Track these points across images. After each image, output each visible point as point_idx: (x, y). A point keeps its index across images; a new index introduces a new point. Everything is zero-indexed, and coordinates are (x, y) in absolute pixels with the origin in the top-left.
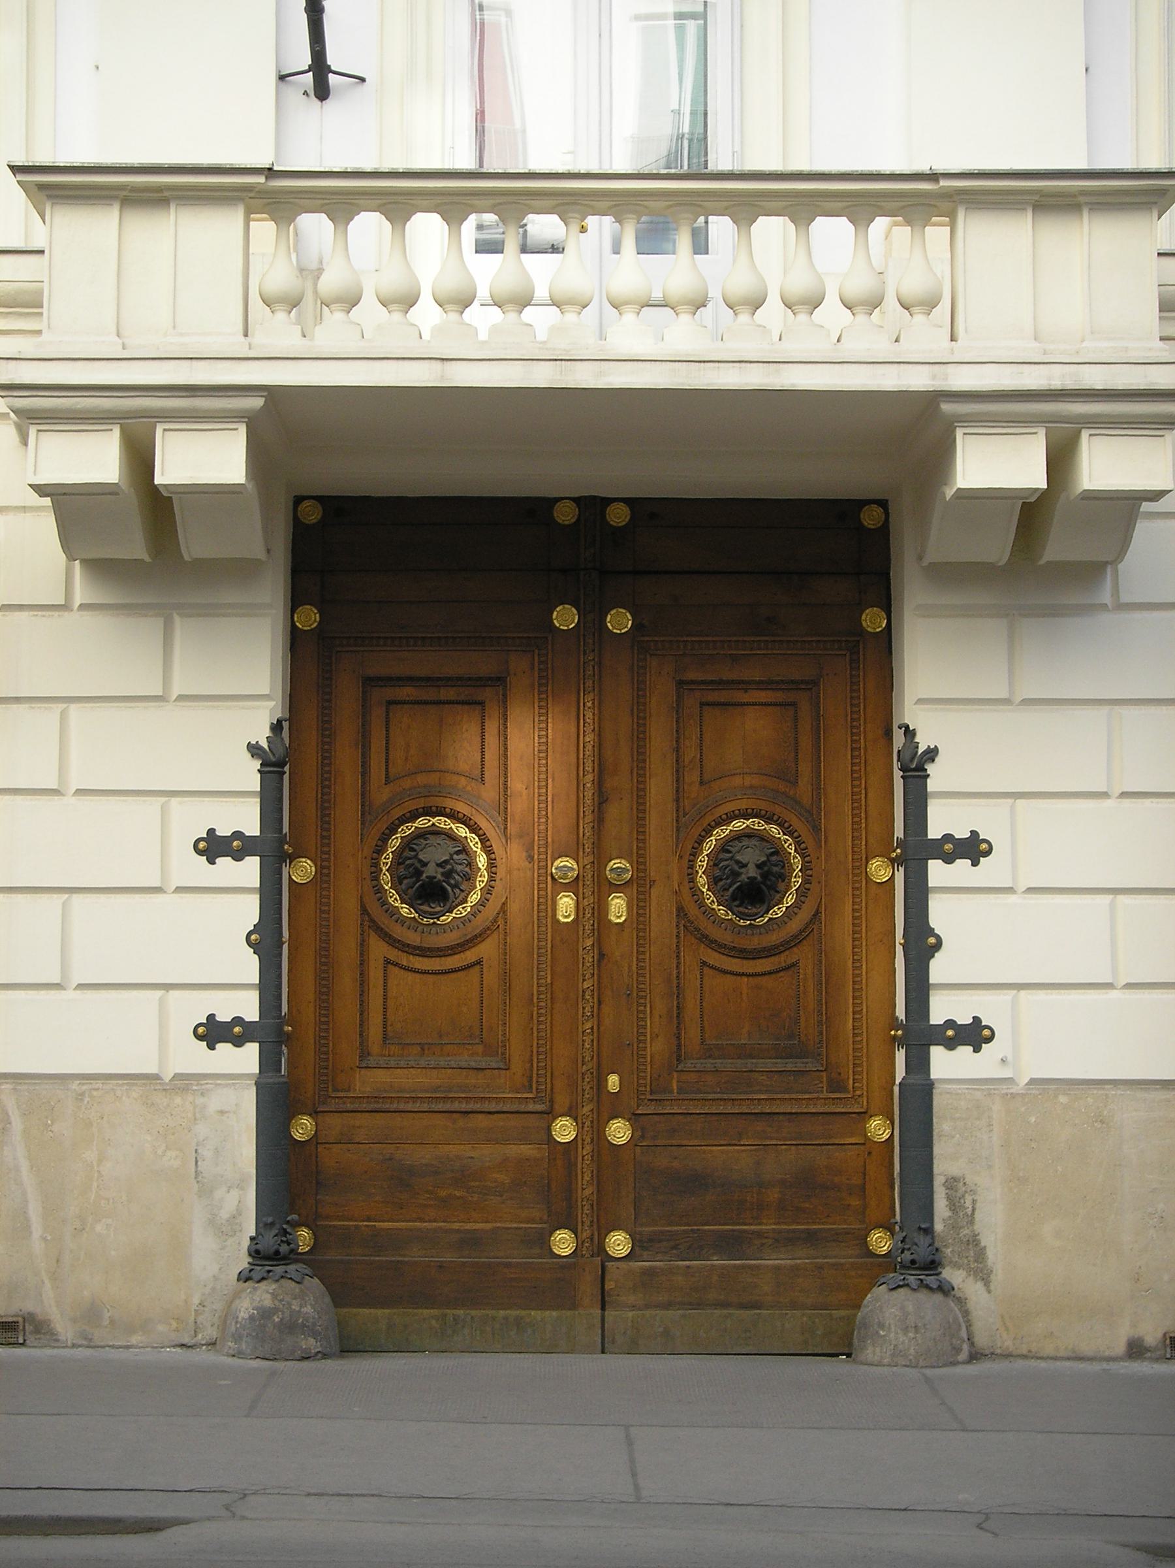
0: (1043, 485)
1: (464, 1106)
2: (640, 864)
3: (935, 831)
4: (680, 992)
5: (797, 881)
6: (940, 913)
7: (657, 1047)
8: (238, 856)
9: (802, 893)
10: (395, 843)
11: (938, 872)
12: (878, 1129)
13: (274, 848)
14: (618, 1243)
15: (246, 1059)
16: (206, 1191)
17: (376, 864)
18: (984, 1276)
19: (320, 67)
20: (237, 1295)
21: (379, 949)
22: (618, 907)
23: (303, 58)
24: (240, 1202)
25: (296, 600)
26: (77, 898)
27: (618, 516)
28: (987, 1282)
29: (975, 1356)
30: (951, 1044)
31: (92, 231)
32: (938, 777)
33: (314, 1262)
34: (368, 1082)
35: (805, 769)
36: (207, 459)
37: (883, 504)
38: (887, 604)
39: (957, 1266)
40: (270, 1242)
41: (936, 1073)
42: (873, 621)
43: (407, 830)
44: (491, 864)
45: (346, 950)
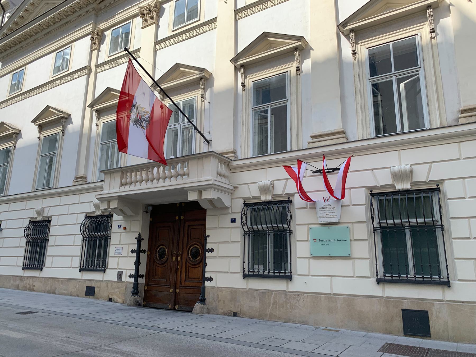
32: (208, 240)
41: (205, 285)
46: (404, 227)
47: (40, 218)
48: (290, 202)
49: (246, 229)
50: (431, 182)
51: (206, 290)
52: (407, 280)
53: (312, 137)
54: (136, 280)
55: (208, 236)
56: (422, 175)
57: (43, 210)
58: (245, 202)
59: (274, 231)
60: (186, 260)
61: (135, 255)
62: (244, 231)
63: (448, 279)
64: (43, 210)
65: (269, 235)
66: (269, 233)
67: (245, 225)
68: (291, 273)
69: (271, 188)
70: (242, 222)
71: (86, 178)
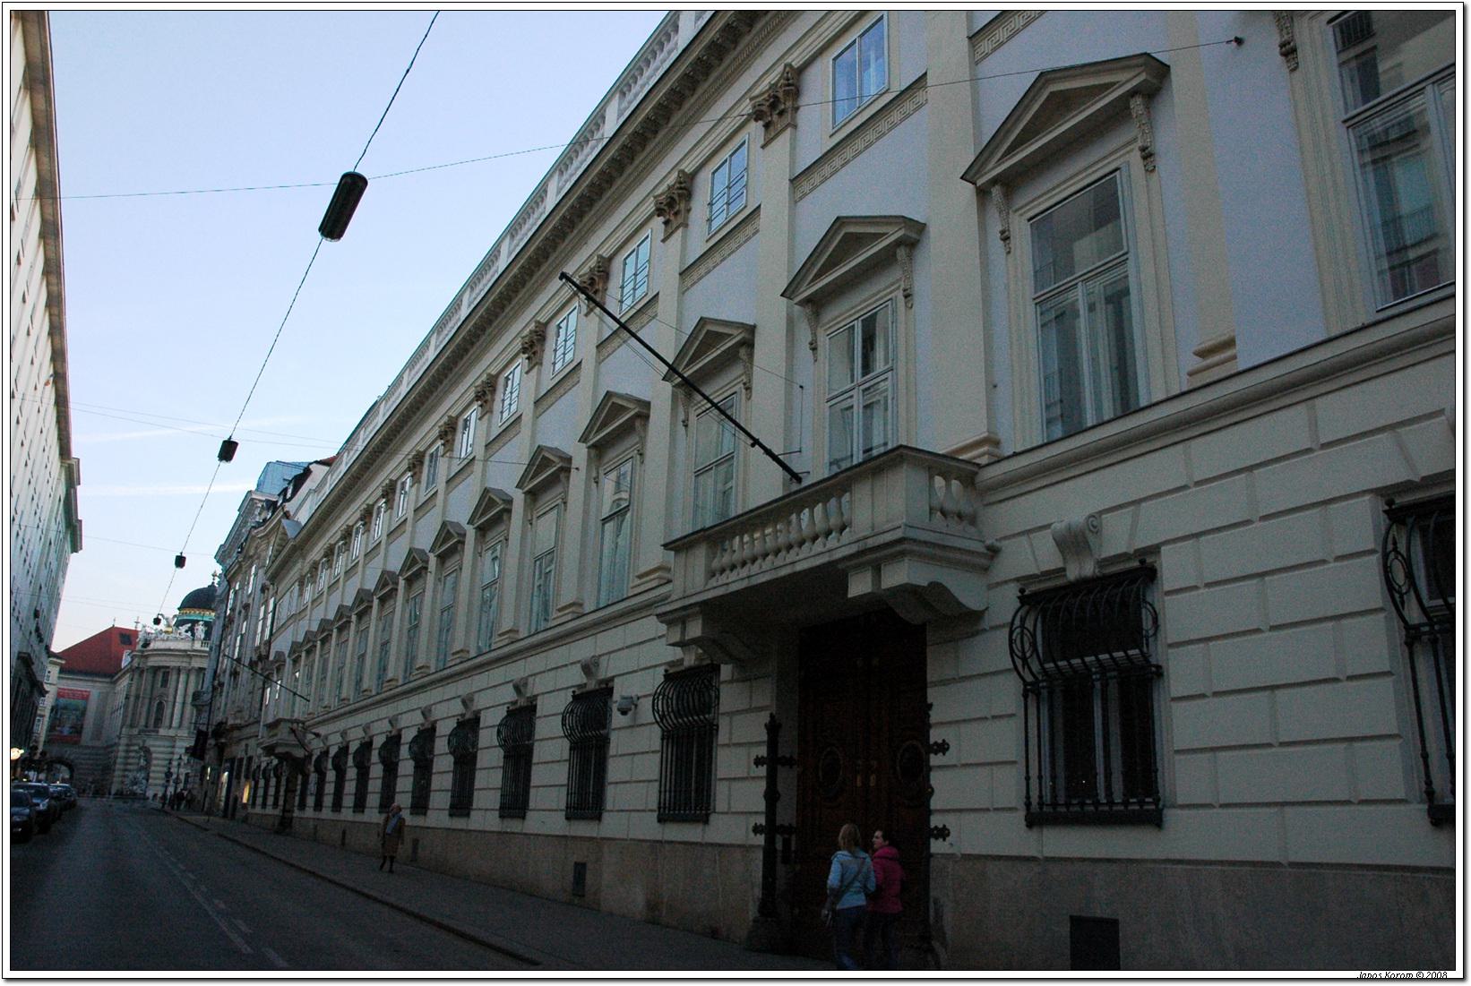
47: (592, 685)
51: (933, 863)
53: (1202, 354)
54: (770, 841)
56: (1118, 540)
57: (1094, 524)
58: (1390, 503)
61: (762, 771)
62: (1407, 627)
64: (326, 738)
71: (997, 443)
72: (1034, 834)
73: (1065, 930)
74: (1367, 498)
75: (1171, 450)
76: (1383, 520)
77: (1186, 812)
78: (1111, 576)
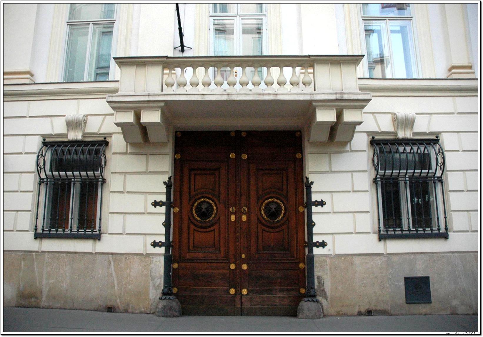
0: (336, 120)
1: (211, 261)
2: (249, 209)
3: (313, 200)
4: (258, 237)
5: (283, 212)
6: (315, 218)
7: (253, 249)
8: (161, 206)
9: (284, 214)
10: (196, 204)
11: (314, 209)
12: (301, 266)
13: (168, 204)
14: (245, 291)
15: (162, 250)
16: (153, 279)
17: (192, 209)
18: (325, 297)
19: (182, 45)
20: (159, 302)
21: (192, 227)
22: (244, 218)
23: (179, 44)
24: (160, 281)
25: (176, 153)
26: (127, 216)
27: (244, 134)
28: (327, 300)
29: (325, 316)
30: (318, 247)
31: (131, 71)
32: (314, 188)
33: (177, 295)
34: (189, 256)
35: (284, 187)
36: (152, 117)
37: (300, 131)
38: (301, 151)
39: (320, 296)
40: (166, 290)
41: (314, 253)
42: (299, 156)
43: (199, 201)
44: (217, 208)
45: (185, 226)
46: (98, 179)
48: (106, 143)
49: (43, 176)
50: (431, 133)
52: (92, 234)
55: (312, 183)
56: (423, 126)
58: (44, 140)
59: (82, 179)
60: (189, 218)
63: (447, 231)
65: (74, 184)
66: (74, 181)
67: (43, 170)
68: (100, 231)
69: (83, 124)
70: (38, 165)
72: (38, 242)
73: (402, 283)
74: (38, 137)
75: (472, 98)
76: (41, 145)
77: (456, 234)
78: (85, 142)
